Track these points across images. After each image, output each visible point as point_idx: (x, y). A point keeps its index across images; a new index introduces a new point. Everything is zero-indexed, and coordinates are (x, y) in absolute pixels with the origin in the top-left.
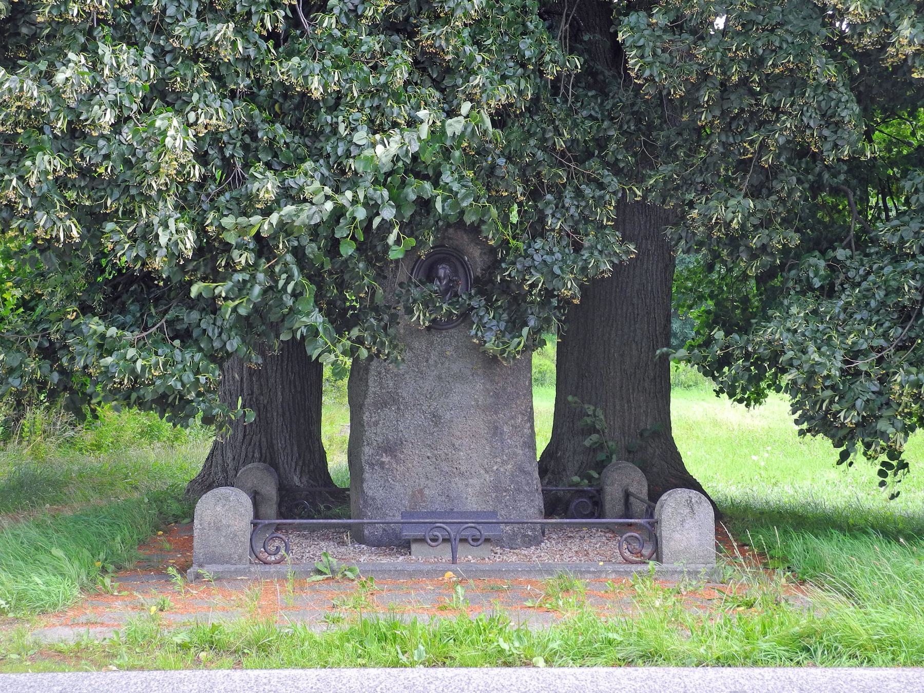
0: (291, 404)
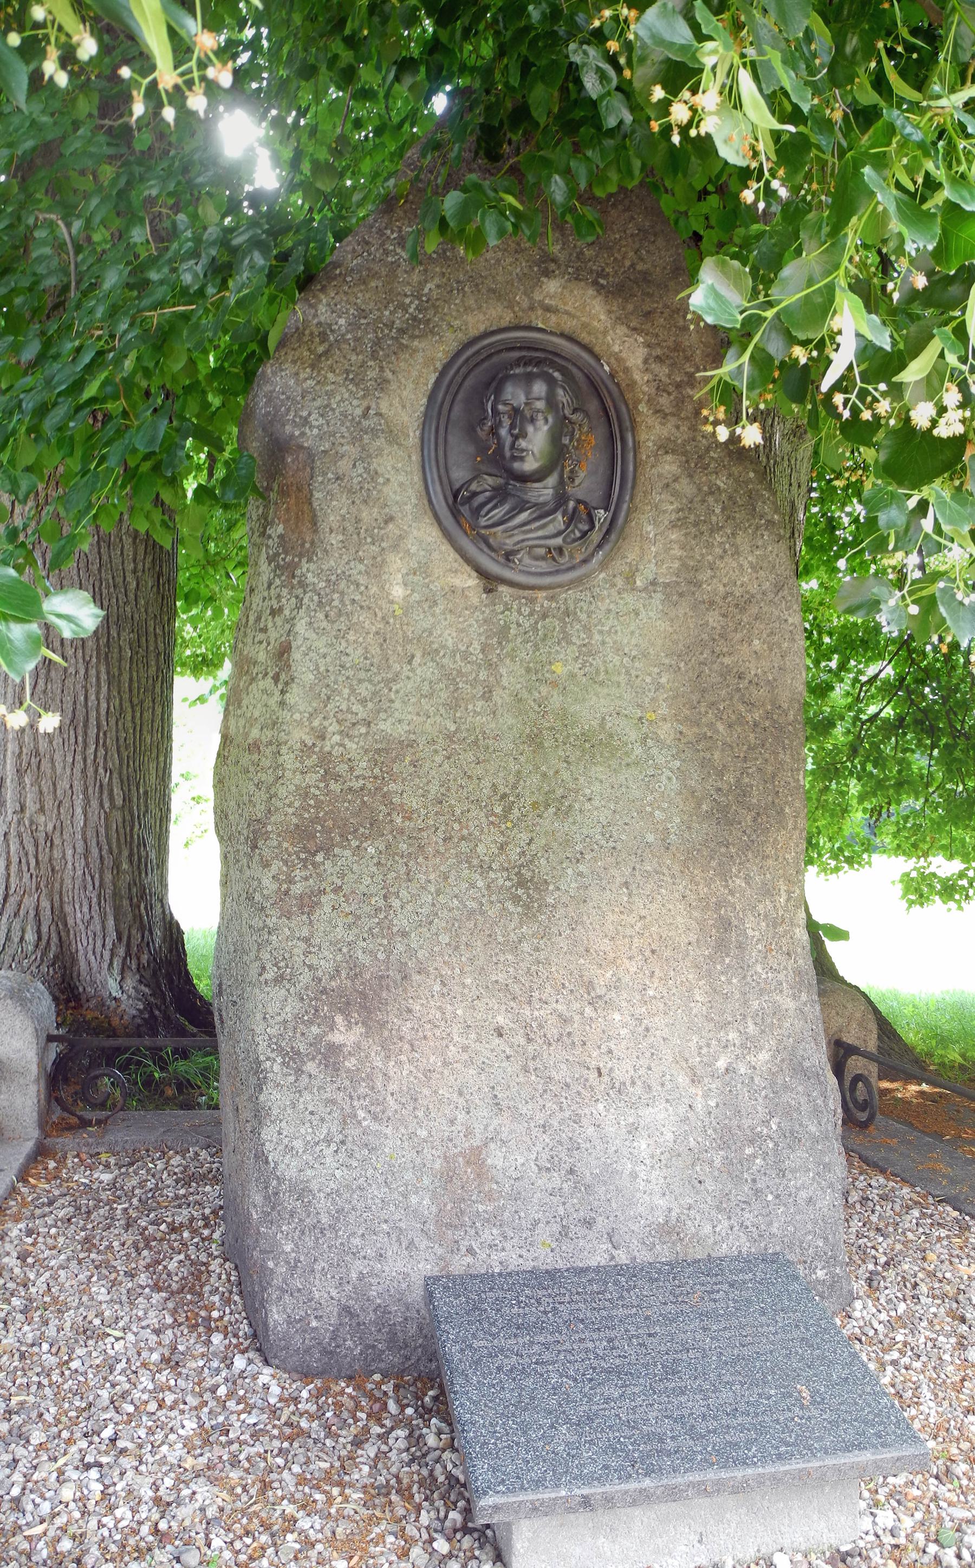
0: (102, 831)
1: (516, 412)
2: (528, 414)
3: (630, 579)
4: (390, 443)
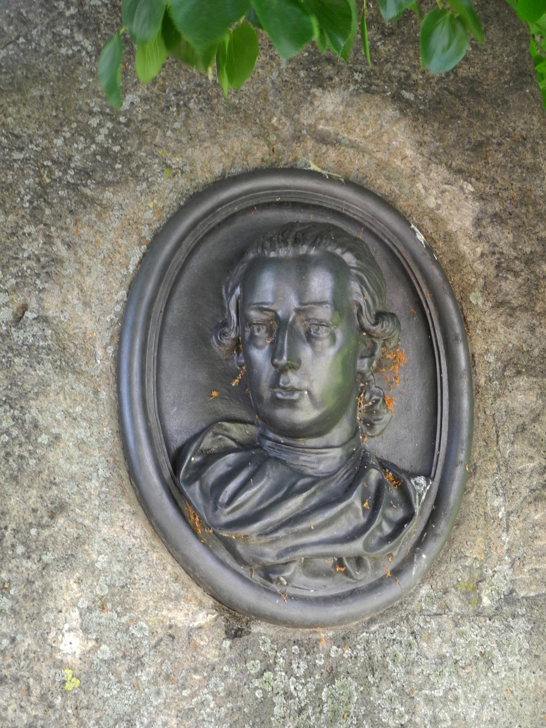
1: (278, 326)
2: (301, 328)
3: (471, 594)
4: (61, 370)
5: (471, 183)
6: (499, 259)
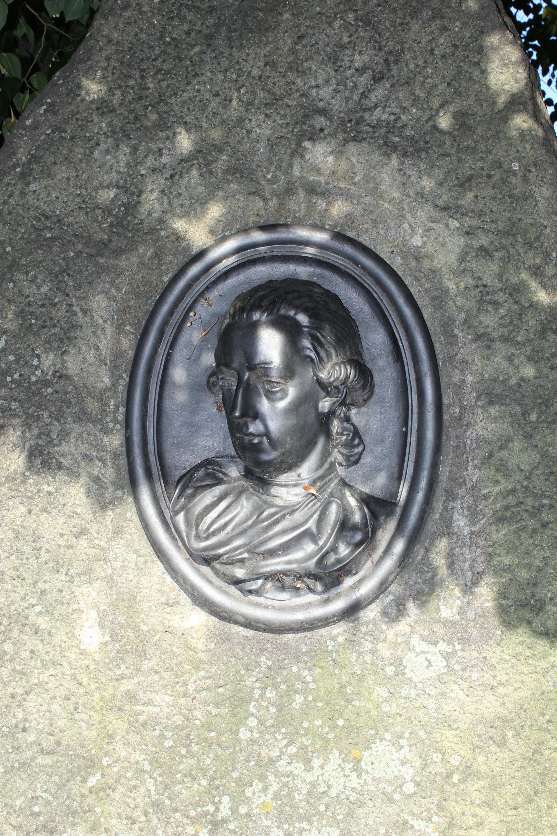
5: (456, 219)
6: (481, 292)
